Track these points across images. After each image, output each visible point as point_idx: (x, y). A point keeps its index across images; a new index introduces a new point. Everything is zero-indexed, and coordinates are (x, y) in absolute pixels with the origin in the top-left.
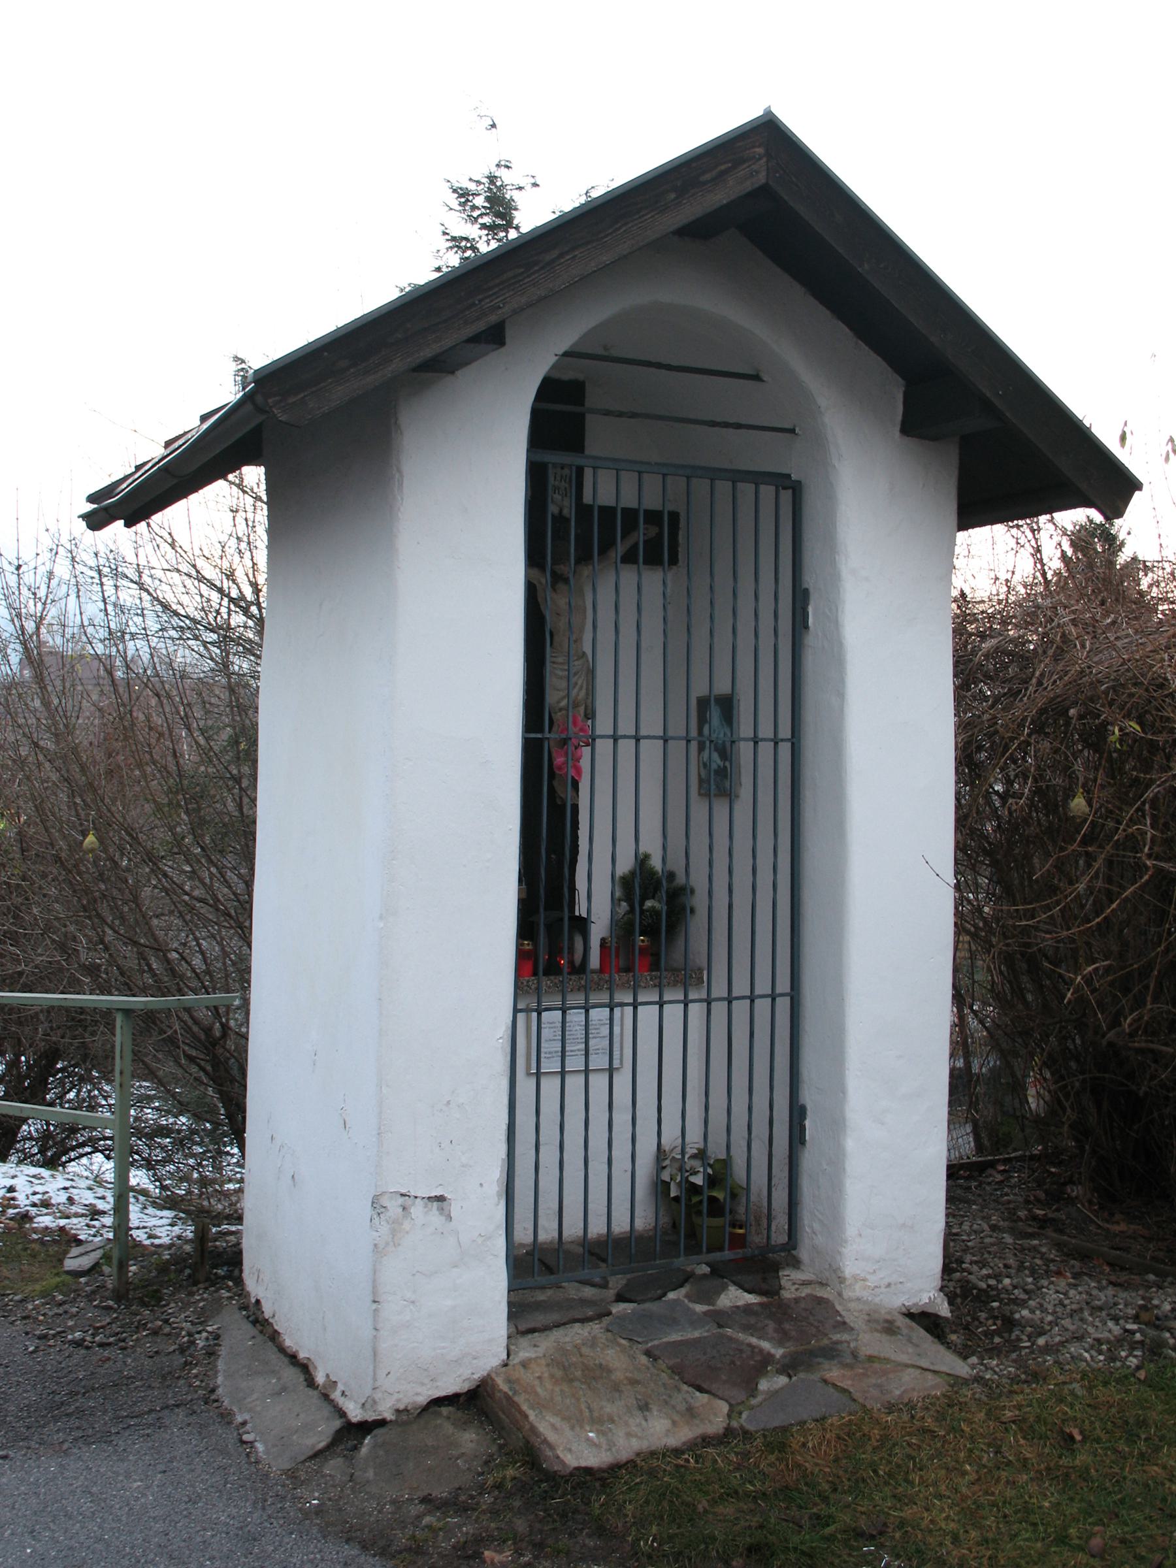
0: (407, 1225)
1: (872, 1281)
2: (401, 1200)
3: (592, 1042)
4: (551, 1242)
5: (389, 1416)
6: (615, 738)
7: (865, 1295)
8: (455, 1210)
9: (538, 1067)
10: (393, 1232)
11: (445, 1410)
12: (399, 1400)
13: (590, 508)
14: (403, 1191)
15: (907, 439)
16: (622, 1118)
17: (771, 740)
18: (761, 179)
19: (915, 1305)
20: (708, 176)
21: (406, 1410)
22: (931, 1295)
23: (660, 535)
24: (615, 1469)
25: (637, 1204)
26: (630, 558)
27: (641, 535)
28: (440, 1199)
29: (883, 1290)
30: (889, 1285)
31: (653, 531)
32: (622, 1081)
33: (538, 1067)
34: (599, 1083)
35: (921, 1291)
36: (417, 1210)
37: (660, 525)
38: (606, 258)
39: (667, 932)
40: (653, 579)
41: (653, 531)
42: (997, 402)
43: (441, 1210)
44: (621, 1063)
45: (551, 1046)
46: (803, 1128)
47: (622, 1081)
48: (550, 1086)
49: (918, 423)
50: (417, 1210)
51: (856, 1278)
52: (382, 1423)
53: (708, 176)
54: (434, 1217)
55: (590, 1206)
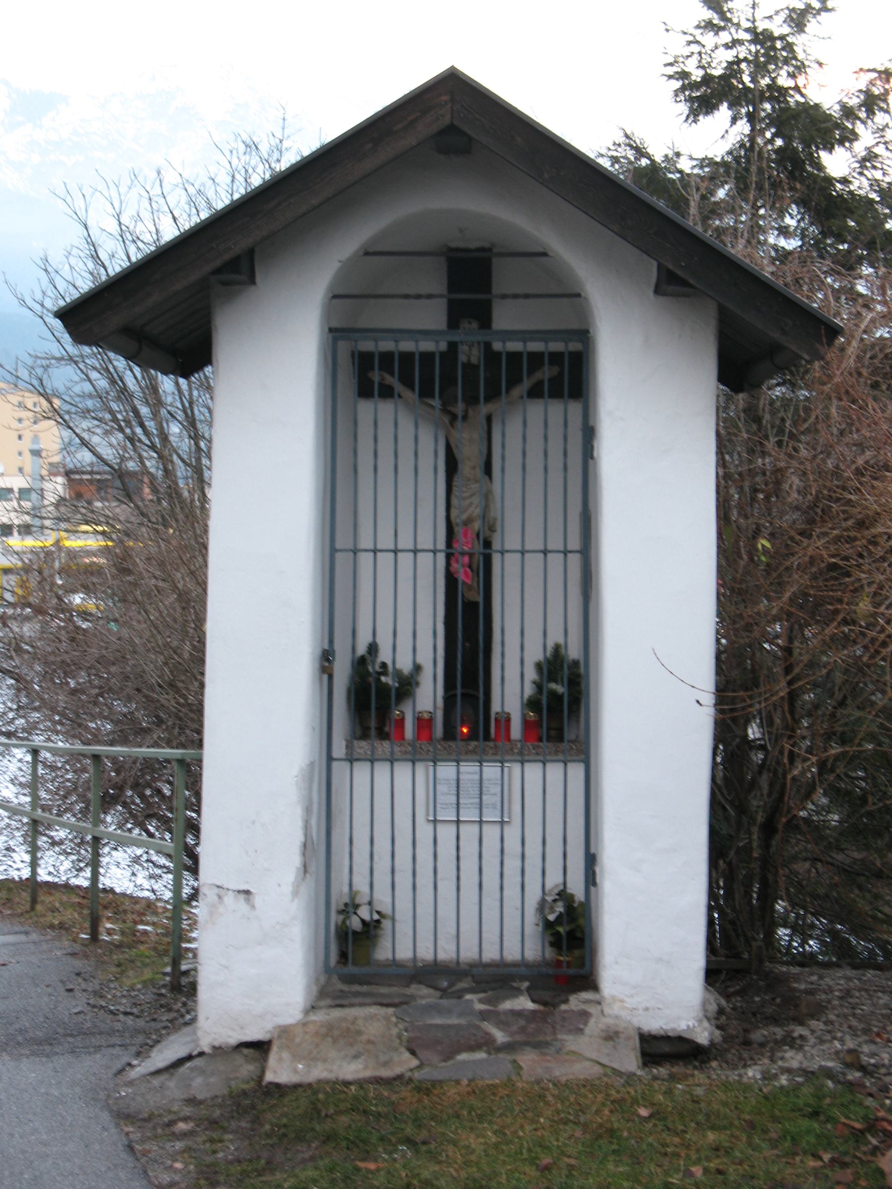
0: (221, 909)
1: (630, 1003)
2: (216, 890)
3: (484, 797)
4: (451, 962)
5: (207, 1049)
6: (355, 551)
7: (624, 1014)
8: (258, 900)
9: (435, 815)
10: (211, 914)
11: (246, 1051)
12: (215, 1039)
13: (499, 354)
14: (219, 884)
15: (662, 299)
16: (512, 865)
17: (541, 551)
18: (447, 120)
19: (674, 1030)
20: (400, 126)
21: (220, 1048)
22: (691, 1024)
23: (561, 374)
24: (296, 1086)
25: (526, 938)
26: (535, 393)
27: (546, 373)
28: (247, 892)
29: (641, 1012)
30: (647, 1009)
31: (555, 370)
32: (512, 834)
33: (435, 815)
34: (491, 833)
35: (679, 1018)
36: (229, 899)
37: (561, 365)
38: (314, 202)
39: (570, 712)
40: (555, 409)
41: (555, 370)
42: (680, 273)
43: (248, 901)
44: (510, 817)
45: (446, 797)
46: (594, 873)
47: (512, 834)
48: (447, 833)
49: (670, 284)
50: (229, 899)
51: (614, 999)
52: (201, 1054)
53: (400, 126)
54: (241, 904)
55: (484, 935)
